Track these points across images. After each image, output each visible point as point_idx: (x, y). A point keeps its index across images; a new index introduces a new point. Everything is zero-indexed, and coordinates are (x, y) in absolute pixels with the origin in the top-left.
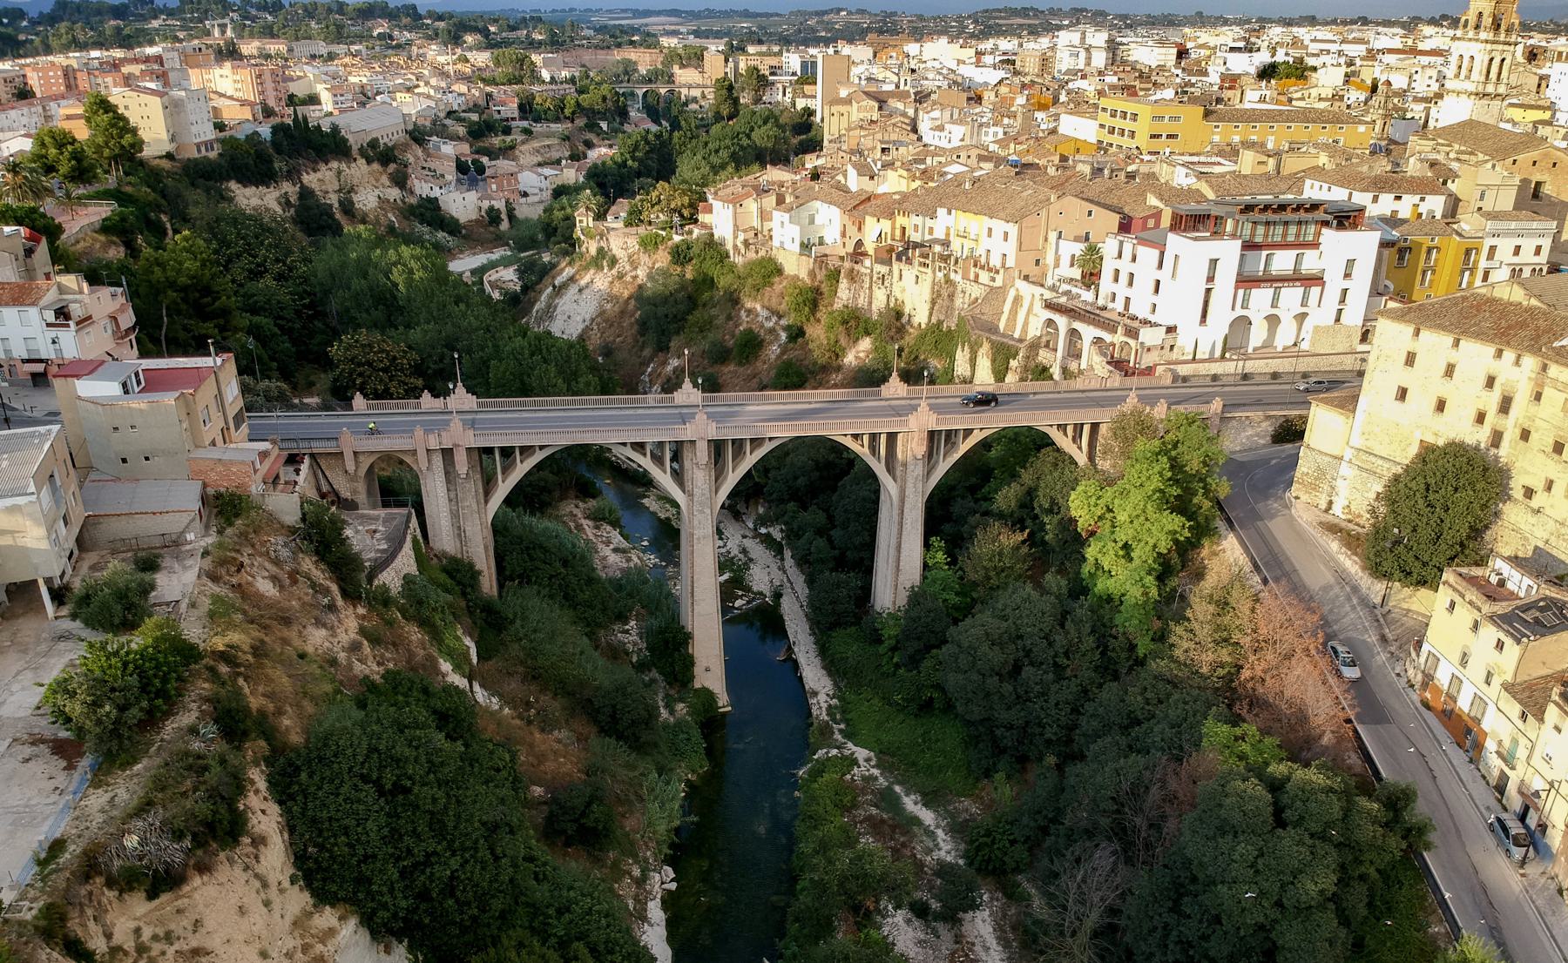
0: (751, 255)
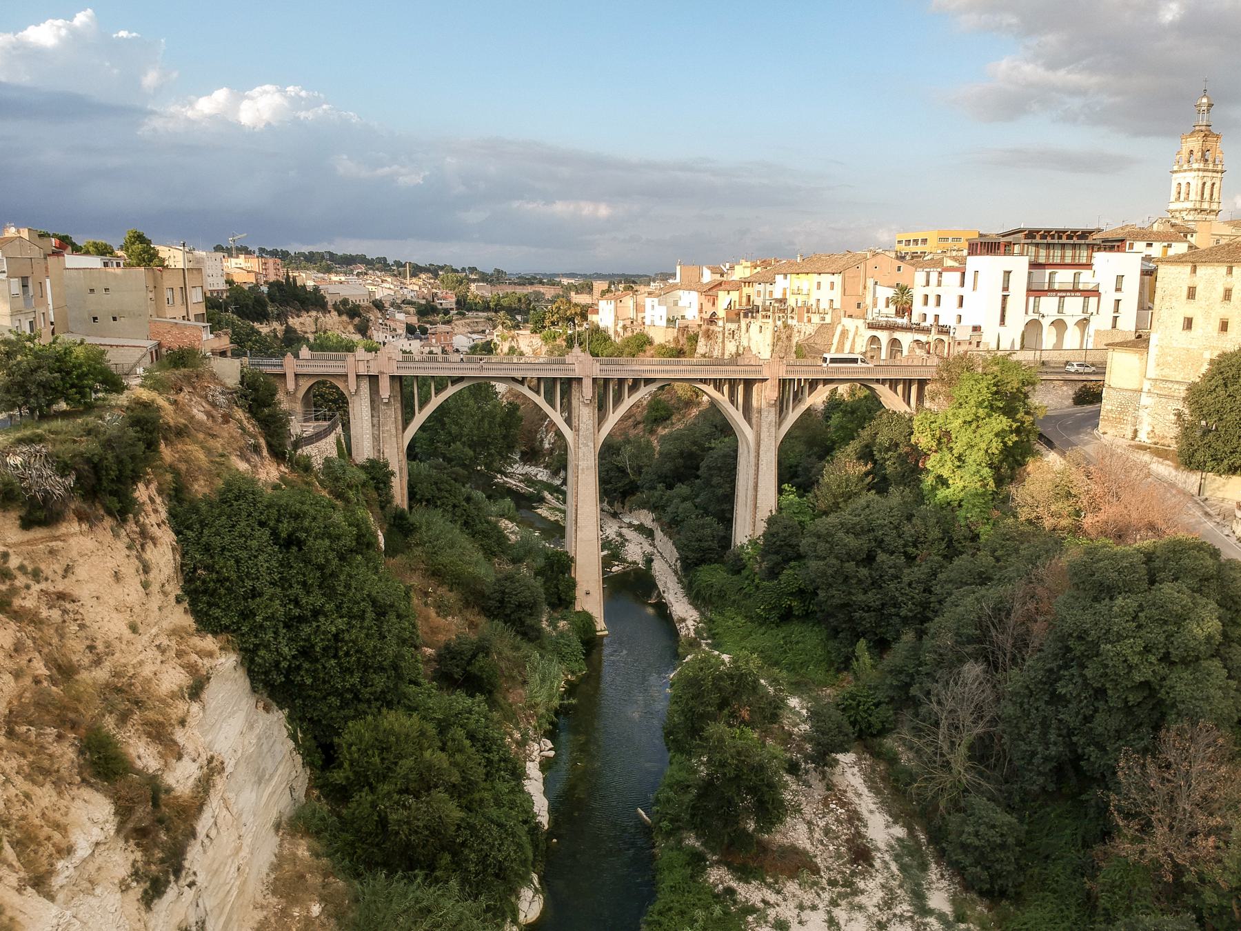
0: (629, 334)
